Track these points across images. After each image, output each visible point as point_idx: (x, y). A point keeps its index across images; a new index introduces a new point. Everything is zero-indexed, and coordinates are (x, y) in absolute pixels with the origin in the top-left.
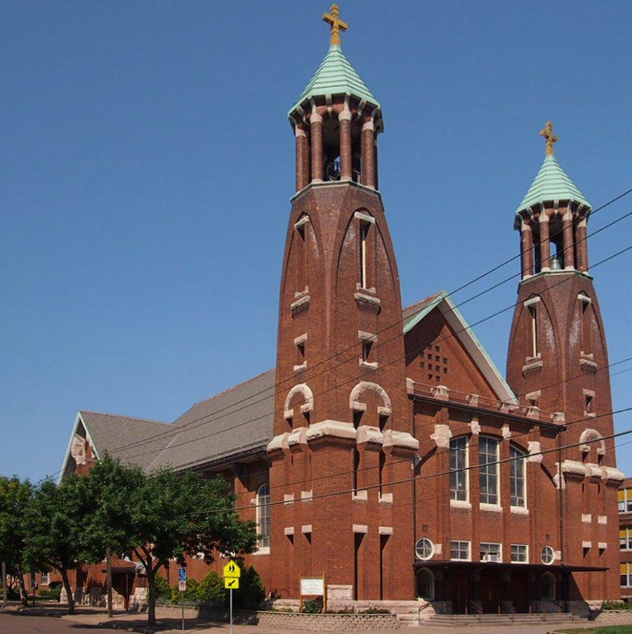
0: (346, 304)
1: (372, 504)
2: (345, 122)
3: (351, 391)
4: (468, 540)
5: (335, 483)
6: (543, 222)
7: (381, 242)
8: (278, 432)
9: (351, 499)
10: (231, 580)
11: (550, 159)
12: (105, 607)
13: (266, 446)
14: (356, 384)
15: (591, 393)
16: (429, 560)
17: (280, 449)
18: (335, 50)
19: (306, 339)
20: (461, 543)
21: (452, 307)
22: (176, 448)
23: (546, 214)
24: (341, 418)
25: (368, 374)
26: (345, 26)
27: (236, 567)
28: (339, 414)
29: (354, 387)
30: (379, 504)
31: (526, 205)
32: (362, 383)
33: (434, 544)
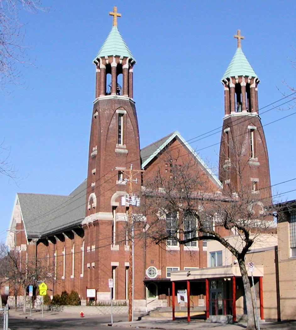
0: (110, 155)
1: (121, 252)
2: (114, 68)
3: (111, 197)
4: (177, 266)
5: (102, 242)
6: (231, 87)
7: (130, 121)
8: (87, 215)
9: (110, 249)
10: (43, 291)
11: (239, 50)
12: (168, 276)
13: (81, 222)
14: (114, 193)
15: (257, 180)
16: (155, 278)
17: (86, 224)
18: (115, 29)
19: (95, 171)
20: (174, 268)
21: (183, 142)
22: (265, 156)
23: (233, 83)
24: (106, 210)
25: (121, 188)
26: (120, 15)
27: (45, 285)
28: (105, 208)
29: (113, 195)
30: (125, 251)
31: (224, 78)
32: (118, 192)
33: (158, 269)
